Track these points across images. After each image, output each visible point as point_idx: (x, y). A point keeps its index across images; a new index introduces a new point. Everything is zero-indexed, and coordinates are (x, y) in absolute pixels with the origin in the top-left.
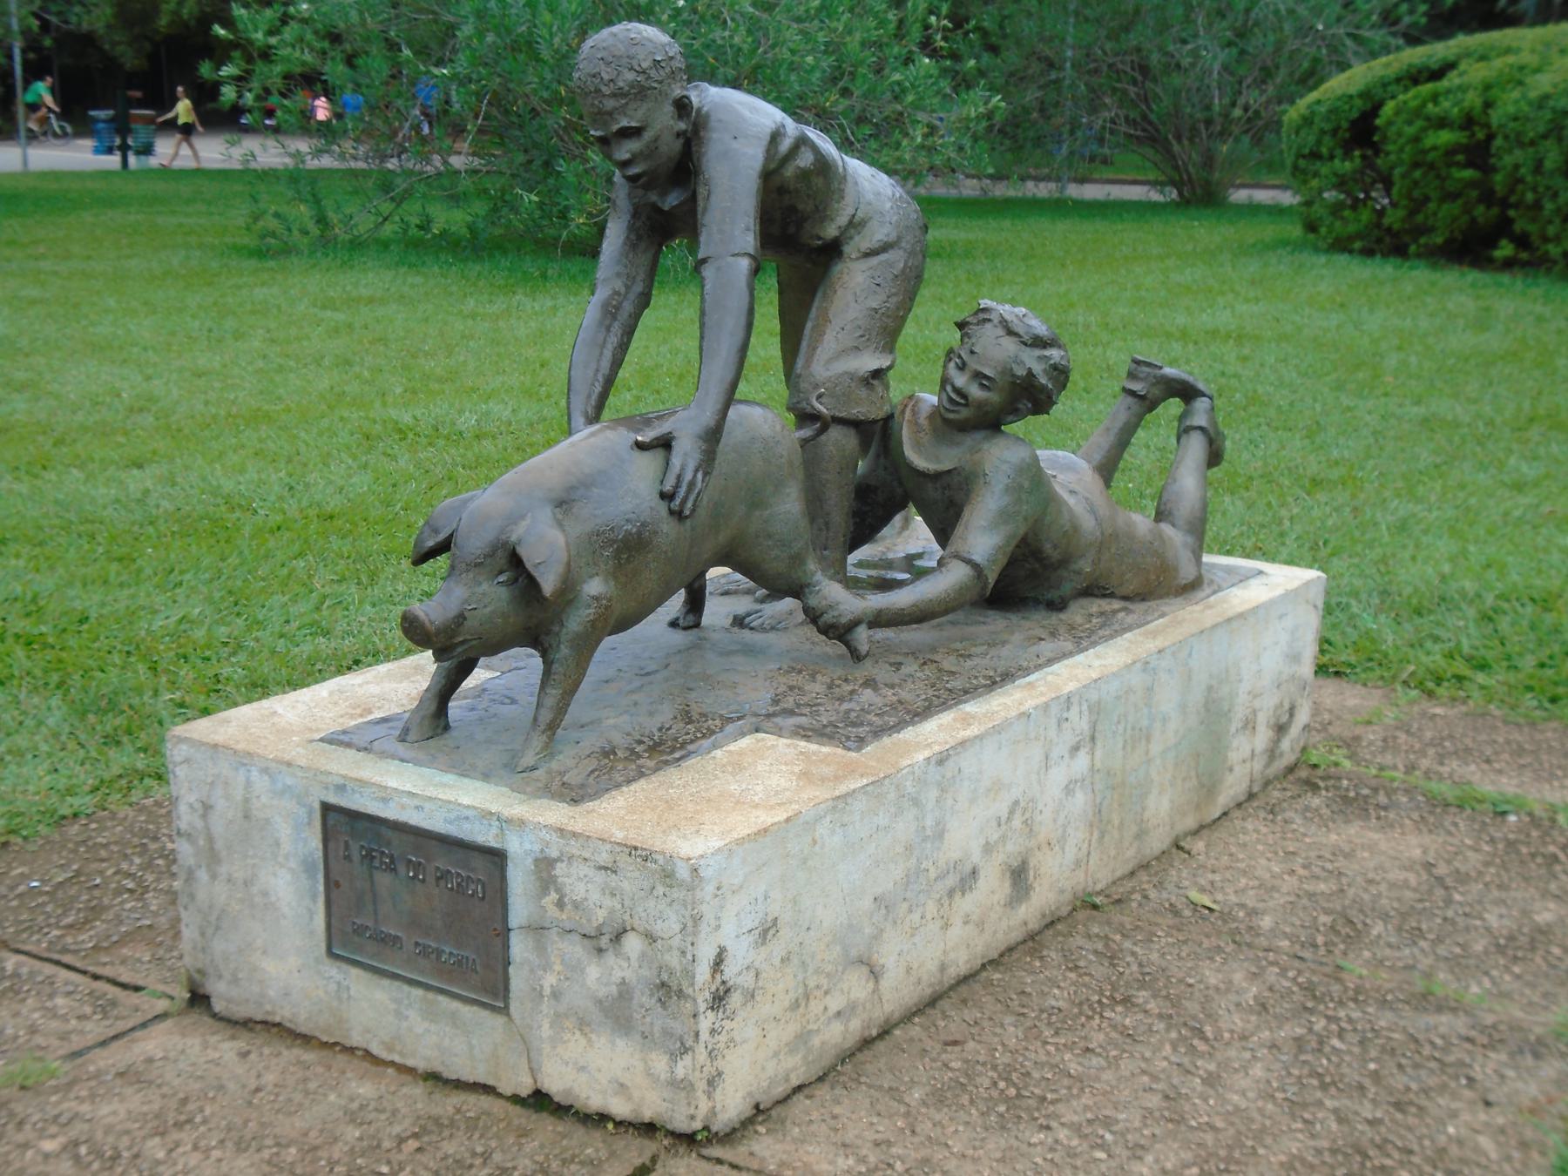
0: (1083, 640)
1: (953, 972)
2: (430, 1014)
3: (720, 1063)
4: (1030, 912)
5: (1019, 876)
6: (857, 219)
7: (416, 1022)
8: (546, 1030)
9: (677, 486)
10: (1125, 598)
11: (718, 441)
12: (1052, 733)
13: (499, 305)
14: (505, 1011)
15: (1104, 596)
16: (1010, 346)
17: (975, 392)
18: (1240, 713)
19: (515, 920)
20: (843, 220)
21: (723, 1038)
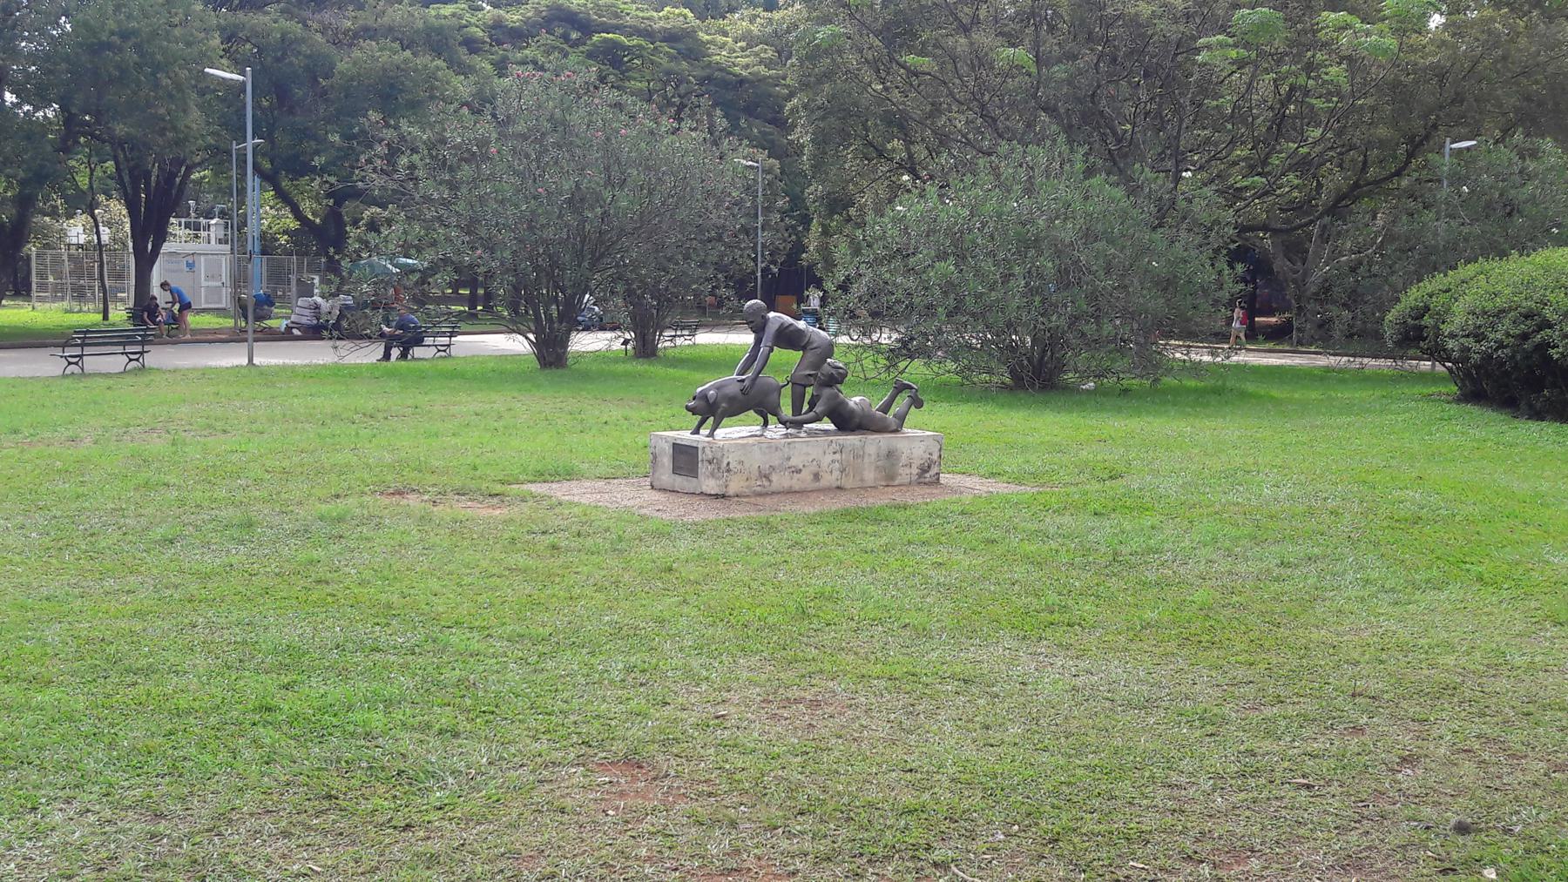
5: (817, 476)
18: (904, 460)
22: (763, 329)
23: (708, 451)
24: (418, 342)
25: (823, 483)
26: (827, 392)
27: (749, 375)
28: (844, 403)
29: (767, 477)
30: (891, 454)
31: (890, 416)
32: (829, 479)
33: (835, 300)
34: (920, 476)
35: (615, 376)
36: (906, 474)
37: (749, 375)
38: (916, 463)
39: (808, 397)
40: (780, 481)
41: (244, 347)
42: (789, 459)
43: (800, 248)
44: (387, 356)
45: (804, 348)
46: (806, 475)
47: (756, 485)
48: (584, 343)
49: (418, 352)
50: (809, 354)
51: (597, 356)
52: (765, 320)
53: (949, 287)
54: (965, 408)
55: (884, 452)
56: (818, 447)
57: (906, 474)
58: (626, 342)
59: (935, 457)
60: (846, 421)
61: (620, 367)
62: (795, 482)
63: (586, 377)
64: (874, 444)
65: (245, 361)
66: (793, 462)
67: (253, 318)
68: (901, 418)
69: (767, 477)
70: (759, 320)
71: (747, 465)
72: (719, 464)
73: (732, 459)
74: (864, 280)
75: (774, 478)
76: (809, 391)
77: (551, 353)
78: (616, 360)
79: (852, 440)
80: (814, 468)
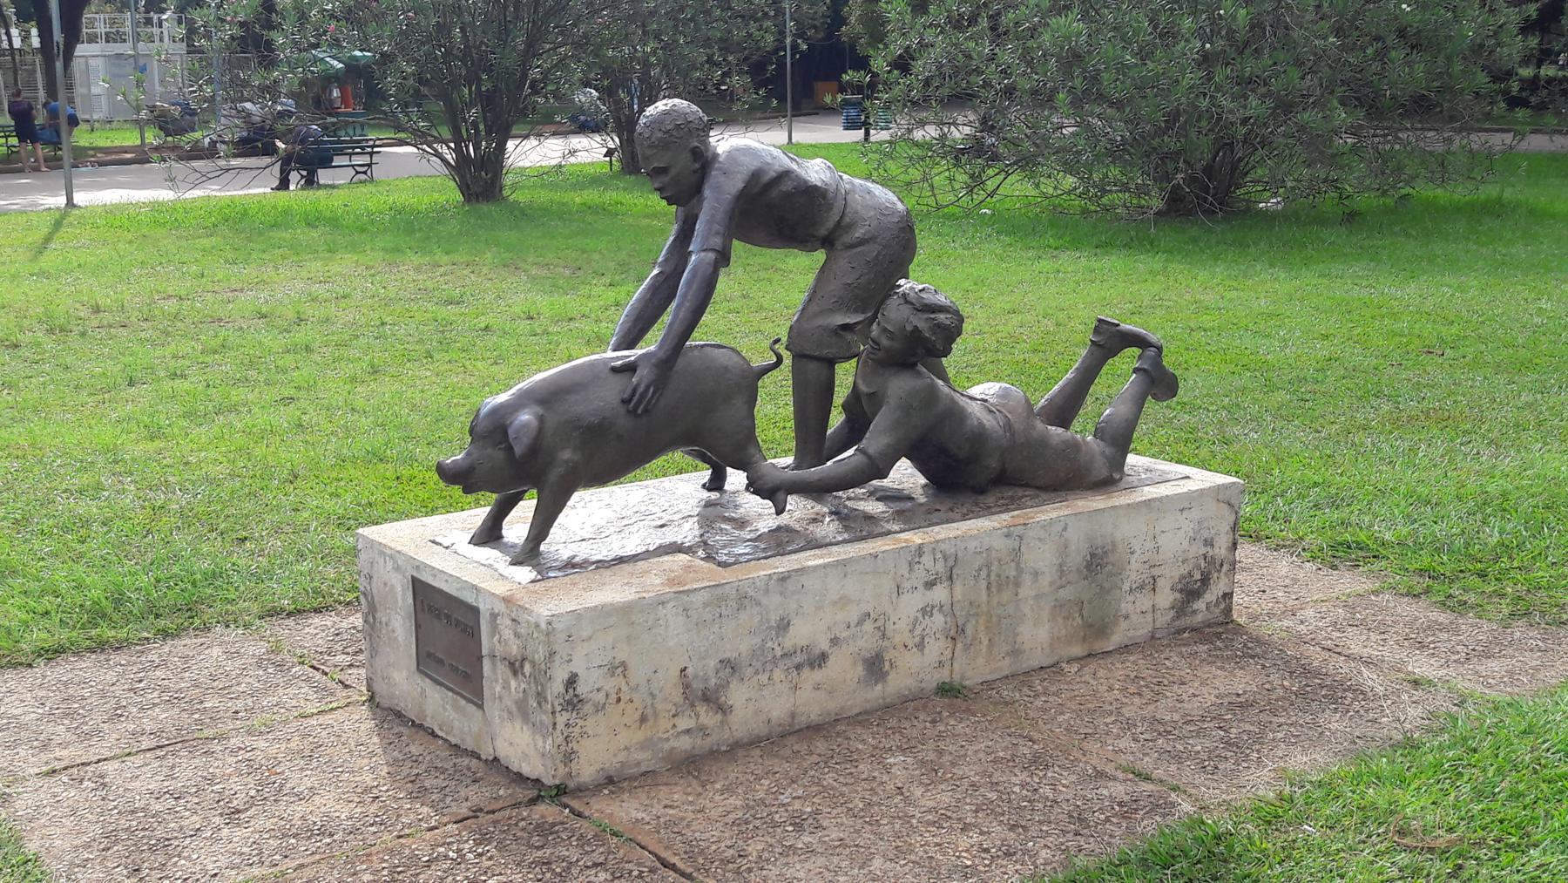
0: (989, 511)
1: (802, 721)
2: (457, 708)
3: (574, 744)
4: (876, 693)
5: (875, 667)
6: (844, 223)
7: (451, 714)
8: (497, 720)
9: (633, 395)
10: (1038, 488)
11: (670, 369)
12: (904, 570)
13: (1046, 264)
14: (481, 707)
15: (1021, 486)
16: (906, 311)
17: (885, 342)
18: (1134, 572)
19: (484, 652)
20: (831, 224)
21: (577, 730)
22: (697, 190)
23: (504, 623)
24: (326, 162)
25: (899, 682)
26: (899, 386)
27: (650, 344)
28: (955, 414)
29: (711, 698)
30: (1099, 562)
31: (1083, 430)
32: (914, 669)
33: (888, 86)
34: (1181, 609)
35: (562, 213)
36: (1140, 612)
37: (650, 344)
38: (1171, 574)
39: (841, 394)
40: (756, 704)
41: (58, 177)
42: (784, 626)
43: (838, 20)
44: (284, 184)
45: (828, 242)
46: (843, 668)
47: (679, 731)
48: (530, 154)
49: (324, 176)
50: (843, 262)
51: (554, 175)
52: (704, 161)
53: (1072, 59)
54: (1114, 262)
55: (1077, 558)
56: (877, 579)
57: (1140, 612)
58: (609, 153)
59: (1221, 550)
60: (967, 468)
61: (591, 196)
62: (809, 698)
63: (524, 216)
64: (1050, 526)
65: (61, 201)
66: (800, 633)
67: (174, 136)
68: (1120, 440)
69: (711, 698)
70: (682, 163)
71: (638, 674)
72: (541, 676)
73: (587, 664)
74: (933, 53)
75: (738, 695)
76: (845, 377)
77: (481, 179)
78: (595, 181)
79: (978, 530)
80: (866, 641)
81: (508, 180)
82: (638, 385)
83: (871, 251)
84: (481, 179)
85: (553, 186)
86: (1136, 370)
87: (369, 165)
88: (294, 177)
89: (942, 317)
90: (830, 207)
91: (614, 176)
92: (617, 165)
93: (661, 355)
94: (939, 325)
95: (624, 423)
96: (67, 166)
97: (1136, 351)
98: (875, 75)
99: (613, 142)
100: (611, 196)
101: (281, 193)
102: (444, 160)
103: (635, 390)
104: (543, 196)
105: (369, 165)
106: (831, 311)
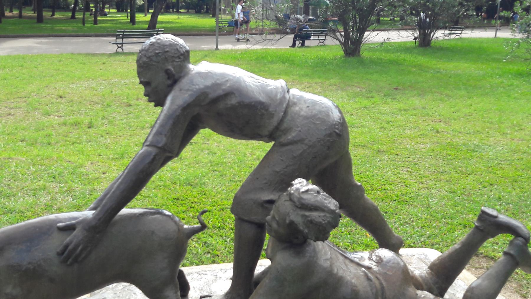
41: (214, 39)
44: (294, 45)
45: (270, 137)
49: (307, 43)
77: (352, 48)
81: (363, 48)
82: (71, 242)
83: (298, 149)
84: (352, 48)
85: (387, 51)
86: (505, 253)
87: (325, 40)
88: (297, 43)
89: (315, 215)
90: (272, 116)
91: (415, 48)
92: (417, 44)
93: (94, 223)
94: (311, 222)
95: (56, 268)
96: (217, 35)
97: (510, 237)
98: (515, 13)
99: (417, 34)
100: (409, 58)
101: (292, 49)
102: (340, 41)
103: (66, 247)
104: (377, 55)
105: (325, 40)
106: (262, 189)
